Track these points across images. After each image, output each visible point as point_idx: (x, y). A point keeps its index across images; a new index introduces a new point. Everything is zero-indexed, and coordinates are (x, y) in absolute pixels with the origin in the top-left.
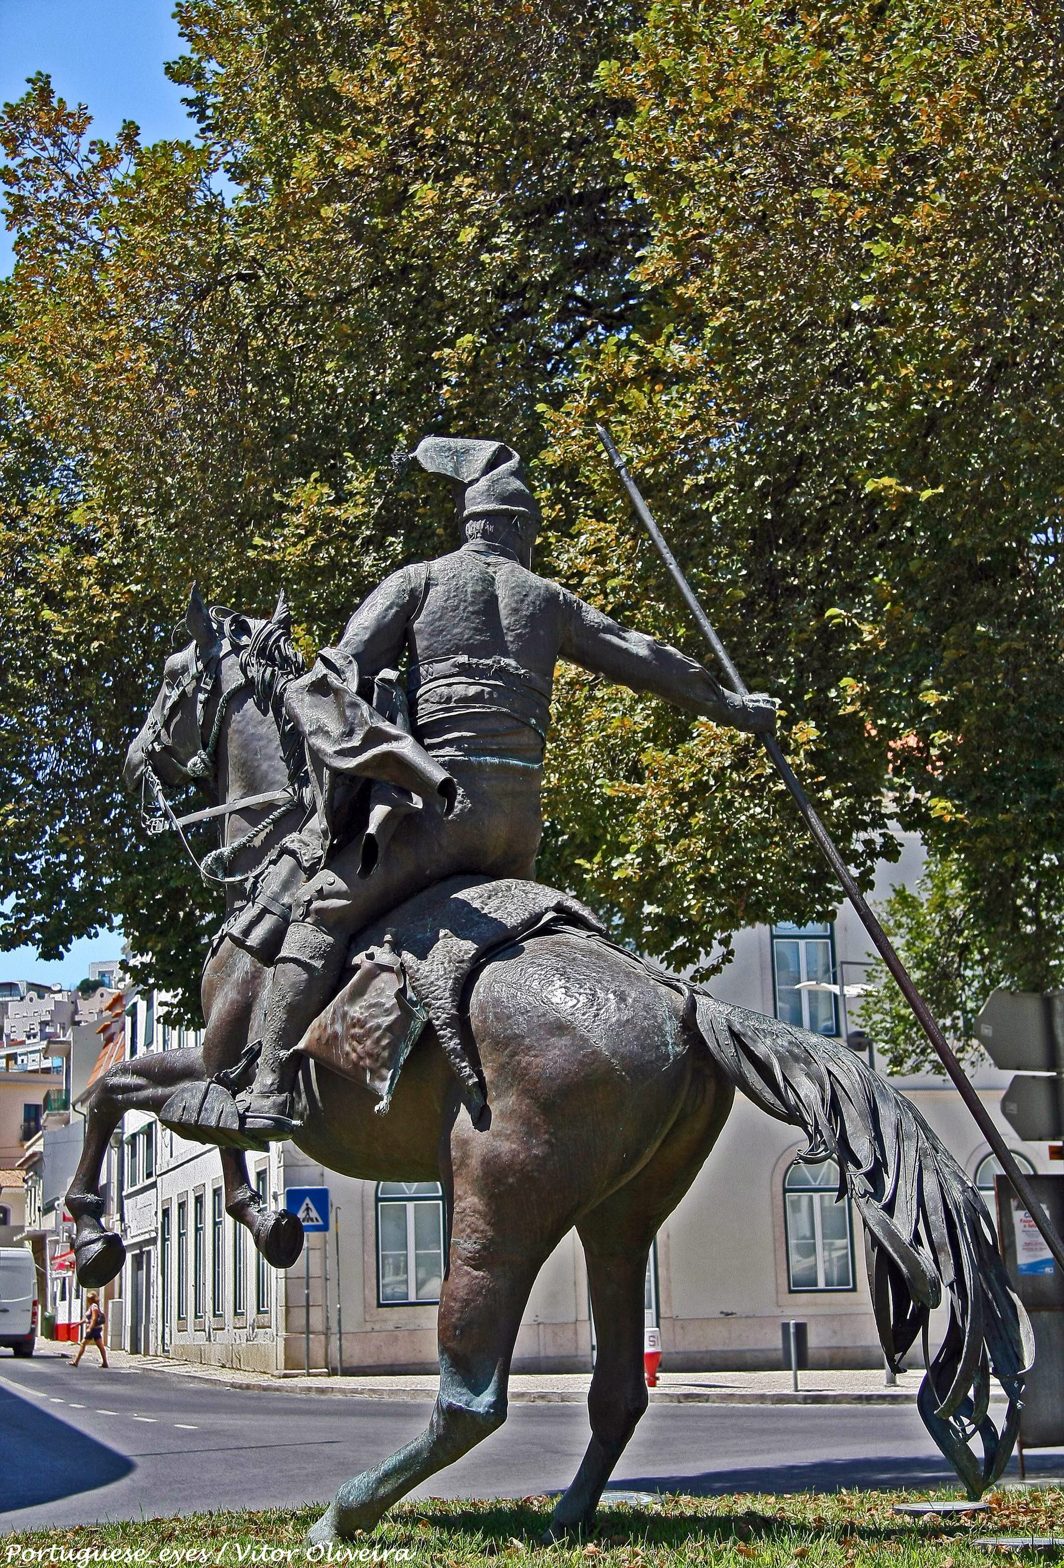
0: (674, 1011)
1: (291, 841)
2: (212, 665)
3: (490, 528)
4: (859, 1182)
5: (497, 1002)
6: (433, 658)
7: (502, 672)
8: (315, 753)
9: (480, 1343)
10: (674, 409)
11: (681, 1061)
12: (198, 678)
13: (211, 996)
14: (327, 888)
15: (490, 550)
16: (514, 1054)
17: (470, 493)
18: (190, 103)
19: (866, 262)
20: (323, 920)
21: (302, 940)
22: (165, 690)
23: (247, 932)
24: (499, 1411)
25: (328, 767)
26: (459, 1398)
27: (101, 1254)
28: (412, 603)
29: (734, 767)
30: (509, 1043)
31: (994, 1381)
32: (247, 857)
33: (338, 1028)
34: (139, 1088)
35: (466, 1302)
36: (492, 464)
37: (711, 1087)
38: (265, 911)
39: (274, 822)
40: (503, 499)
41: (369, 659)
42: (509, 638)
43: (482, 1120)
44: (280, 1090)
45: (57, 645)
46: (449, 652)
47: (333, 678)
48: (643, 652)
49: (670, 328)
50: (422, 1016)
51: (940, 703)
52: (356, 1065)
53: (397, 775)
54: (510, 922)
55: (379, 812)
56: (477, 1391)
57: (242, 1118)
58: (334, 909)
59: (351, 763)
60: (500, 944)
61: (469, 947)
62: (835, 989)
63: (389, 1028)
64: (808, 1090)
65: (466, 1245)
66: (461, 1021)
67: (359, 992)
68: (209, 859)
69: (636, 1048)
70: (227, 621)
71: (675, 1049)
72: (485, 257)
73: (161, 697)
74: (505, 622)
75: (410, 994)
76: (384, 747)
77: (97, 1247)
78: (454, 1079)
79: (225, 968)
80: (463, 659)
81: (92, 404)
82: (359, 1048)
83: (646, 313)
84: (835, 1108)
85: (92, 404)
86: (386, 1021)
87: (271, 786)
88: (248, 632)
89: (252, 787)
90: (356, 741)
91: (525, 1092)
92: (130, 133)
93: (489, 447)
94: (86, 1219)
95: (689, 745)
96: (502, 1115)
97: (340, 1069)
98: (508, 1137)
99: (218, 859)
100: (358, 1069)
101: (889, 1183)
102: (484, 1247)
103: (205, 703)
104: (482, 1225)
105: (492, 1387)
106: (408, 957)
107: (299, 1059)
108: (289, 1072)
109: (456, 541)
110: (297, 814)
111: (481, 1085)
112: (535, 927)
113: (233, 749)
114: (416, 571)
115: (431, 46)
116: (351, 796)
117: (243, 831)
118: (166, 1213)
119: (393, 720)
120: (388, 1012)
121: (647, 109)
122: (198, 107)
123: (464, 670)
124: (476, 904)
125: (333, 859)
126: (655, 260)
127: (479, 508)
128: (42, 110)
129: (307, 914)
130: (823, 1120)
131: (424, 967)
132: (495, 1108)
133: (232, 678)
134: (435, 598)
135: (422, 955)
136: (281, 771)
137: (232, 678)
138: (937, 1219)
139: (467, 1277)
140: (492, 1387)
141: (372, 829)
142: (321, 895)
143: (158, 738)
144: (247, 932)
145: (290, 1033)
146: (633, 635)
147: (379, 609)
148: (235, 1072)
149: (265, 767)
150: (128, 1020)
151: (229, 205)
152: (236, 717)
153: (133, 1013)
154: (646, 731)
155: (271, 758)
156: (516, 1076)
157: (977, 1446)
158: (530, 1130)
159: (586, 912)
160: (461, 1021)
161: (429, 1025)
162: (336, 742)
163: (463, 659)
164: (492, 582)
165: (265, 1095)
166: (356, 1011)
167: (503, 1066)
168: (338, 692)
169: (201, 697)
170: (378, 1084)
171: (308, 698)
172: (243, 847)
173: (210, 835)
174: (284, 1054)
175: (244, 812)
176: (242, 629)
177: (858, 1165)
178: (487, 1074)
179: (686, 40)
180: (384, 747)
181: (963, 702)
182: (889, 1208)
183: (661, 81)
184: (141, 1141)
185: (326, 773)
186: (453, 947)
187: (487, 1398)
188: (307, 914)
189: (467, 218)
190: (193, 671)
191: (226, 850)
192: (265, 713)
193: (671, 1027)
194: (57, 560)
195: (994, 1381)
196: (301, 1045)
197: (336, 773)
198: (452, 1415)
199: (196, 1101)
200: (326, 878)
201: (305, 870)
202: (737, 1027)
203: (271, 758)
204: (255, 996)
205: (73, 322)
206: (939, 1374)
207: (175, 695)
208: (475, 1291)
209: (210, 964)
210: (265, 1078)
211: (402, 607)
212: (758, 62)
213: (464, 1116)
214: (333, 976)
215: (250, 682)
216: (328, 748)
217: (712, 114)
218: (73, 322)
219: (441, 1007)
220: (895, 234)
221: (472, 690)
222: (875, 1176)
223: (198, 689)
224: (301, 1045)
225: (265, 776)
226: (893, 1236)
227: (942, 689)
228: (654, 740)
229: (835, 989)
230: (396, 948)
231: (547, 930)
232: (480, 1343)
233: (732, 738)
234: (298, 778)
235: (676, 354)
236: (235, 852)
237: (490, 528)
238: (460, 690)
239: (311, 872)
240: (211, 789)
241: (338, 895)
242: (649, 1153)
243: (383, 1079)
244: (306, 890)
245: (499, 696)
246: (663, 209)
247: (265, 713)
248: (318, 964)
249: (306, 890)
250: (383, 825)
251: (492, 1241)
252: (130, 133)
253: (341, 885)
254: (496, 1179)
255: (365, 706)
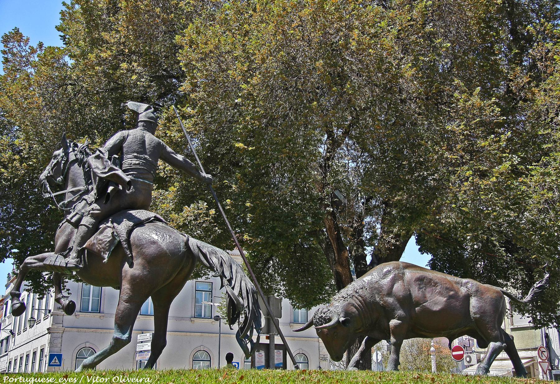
0: (183, 241)
1: (85, 197)
2: (67, 154)
3: (145, 125)
4: (225, 282)
5: (138, 236)
6: (128, 153)
7: (145, 159)
8: (95, 173)
9: (125, 322)
10: (187, 125)
11: (184, 252)
12: (62, 157)
13: (58, 239)
14: (94, 208)
15: (145, 129)
16: (141, 249)
17: (140, 116)
18: (61, 36)
19: (240, 89)
20: (93, 216)
21: (87, 221)
22: (53, 160)
23: (71, 218)
24: (129, 339)
25: (98, 176)
26: (118, 335)
27: (19, 307)
28: (124, 140)
29: (194, 220)
30: (140, 246)
31: (255, 330)
32: (71, 203)
33: (95, 241)
34: (35, 263)
35: (123, 311)
36: (146, 110)
37: (191, 261)
38: (77, 214)
39: (80, 195)
40: (149, 118)
41: (111, 151)
42: (147, 151)
43: (131, 266)
44: (77, 258)
45: (5, 179)
46: (132, 152)
47: (101, 155)
48: (181, 159)
49: (188, 105)
50: (118, 239)
51: (250, 206)
52: (99, 250)
53: (115, 179)
54: (142, 219)
55: (111, 188)
56: (124, 334)
57: (67, 264)
58: (96, 213)
59: (105, 175)
60: (139, 223)
61: (131, 224)
62: (212, 304)
63: (109, 242)
64: (215, 260)
65: (125, 297)
66: (128, 240)
67: (102, 232)
68: (61, 204)
69: (173, 248)
70: (72, 144)
71: (183, 249)
72: (138, 83)
73: (51, 163)
74: (147, 147)
75: (115, 233)
76: (114, 172)
77: (18, 305)
78: (126, 255)
79: (63, 231)
80: (136, 154)
81: (25, 112)
82: (100, 246)
83: (182, 100)
84: (221, 265)
85: (25, 112)
86: (109, 240)
87: (80, 185)
88: (77, 147)
89: (75, 186)
90: (106, 170)
91: (143, 258)
92: (41, 45)
93: (146, 106)
94: (16, 298)
95: (182, 213)
96: (137, 264)
97: (95, 252)
98: (138, 270)
99: (63, 204)
100: (100, 252)
101: (233, 282)
102: (129, 298)
103: (64, 164)
104: (129, 292)
105: (128, 333)
106: (115, 224)
107: (83, 249)
108: (80, 253)
109: (135, 126)
110: (87, 192)
111: (132, 257)
112: (148, 221)
113: (70, 176)
114: (125, 132)
115: (131, 27)
116: (103, 184)
117: (71, 197)
118: (10, 363)
119: (116, 166)
120: (109, 237)
121: (186, 48)
122: (63, 38)
123: (136, 157)
124: (134, 214)
125: (97, 201)
126: (185, 86)
127: (143, 119)
128: (16, 36)
129: (89, 214)
130: (218, 267)
131: (120, 227)
132: (135, 262)
133: (72, 157)
134: (129, 139)
135: (119, 224)
136: (83, 182)
137: (72, 157)
138: (244, 292)
139: (124, 305)
140: (128, 333)
141: (109, 191)
142: (93, 209)
143: (49, 173)
144: (71, 218)
145: (81, 243)
146: (179, 155)
147: (113, 141)
148: (65, 253)
149: (79, 181)
150: (5, 306)
151: (69, 65)
152: (72, 167)
153: (7, 304)
154: (173, 209)
155: (81, 178)
156: (141, 254)
157: (249, 346)
158: (144, 268)
159: (162, 218)
160: (128, 240)
161: (120, 242)
162: (101, 170)
163: (136, 154)
164: (144, 137)
165: (73, 259)
166: (100, 237)
167: (138, 252)
168: (102, 158)
169: (63, 162)
170: (104, 255)
171: (94, 160)
172: (71, 201)
173: (61, 197)
174: (80, 248)
175: (71, 192)
176: (76, 145)
177: (226, 278)
178: (134, 254)
179: (198, 33)
180: (114, 172)
181: (256, 206)
182: (233, 288)
183: (192, 42)
184: (5, 342)
185: (98, 178)
186: (126, 224)
187: (126, 335)
188: (89, 214)
189: (136, 73)
190: (61, 155)
191: (66, 202)
192: (80, 167)
193: (182, 244)
194: (7, 155)
195: (255, 330)
196: (84, 246)
197: (101, 178)
198: (117, 340)
199: (54, 259)
200: (95, 206)
201: (89, 204)
202: (199, 245)
203: (81, 178)
204: (71, 238)
205: (22, 89)
206: (241, 329)
207: (55, 161)
208: (126, 309)
209: (58, 231)
210: (73, 254)
211: (121, 140)
212: (217, 39)
213: (126, 265)
214: (93, 230)
215: (77, 159)
216: (98, 171)
217: (204, 50)
218: (22, 89)
219: (124, 236)
220: (248, 83)
221: (137, 162)
222: (230, 281)
223: (62, 160)
224: (84, 246)
225: (78, 183)
226: (233, 294)
227: (251, 203)
228: (174, 211)
229: (212, 304)
230: (112, 223)
231: (152, 222)
232: (125, 322)
233: (194, 212)
234: (88, 183)
235: (189, 110)
236: (68, 202)
237: (145, 125)
238: (134, 162)
239: (90, 204)
240: (63, 186)
241: (97, 210)
242: (174, 275)
243: (106, 254)
244: (89, 208)
245: (144, 164)
246: (189, 73)
247: (80, 167)
248: (91, 226)
249: (89, 208)
250: (112, 191)
251: (131, 296)
252: (41, 45)
253: (98, 207)
254: (135, 281)
255: (109, 162)
